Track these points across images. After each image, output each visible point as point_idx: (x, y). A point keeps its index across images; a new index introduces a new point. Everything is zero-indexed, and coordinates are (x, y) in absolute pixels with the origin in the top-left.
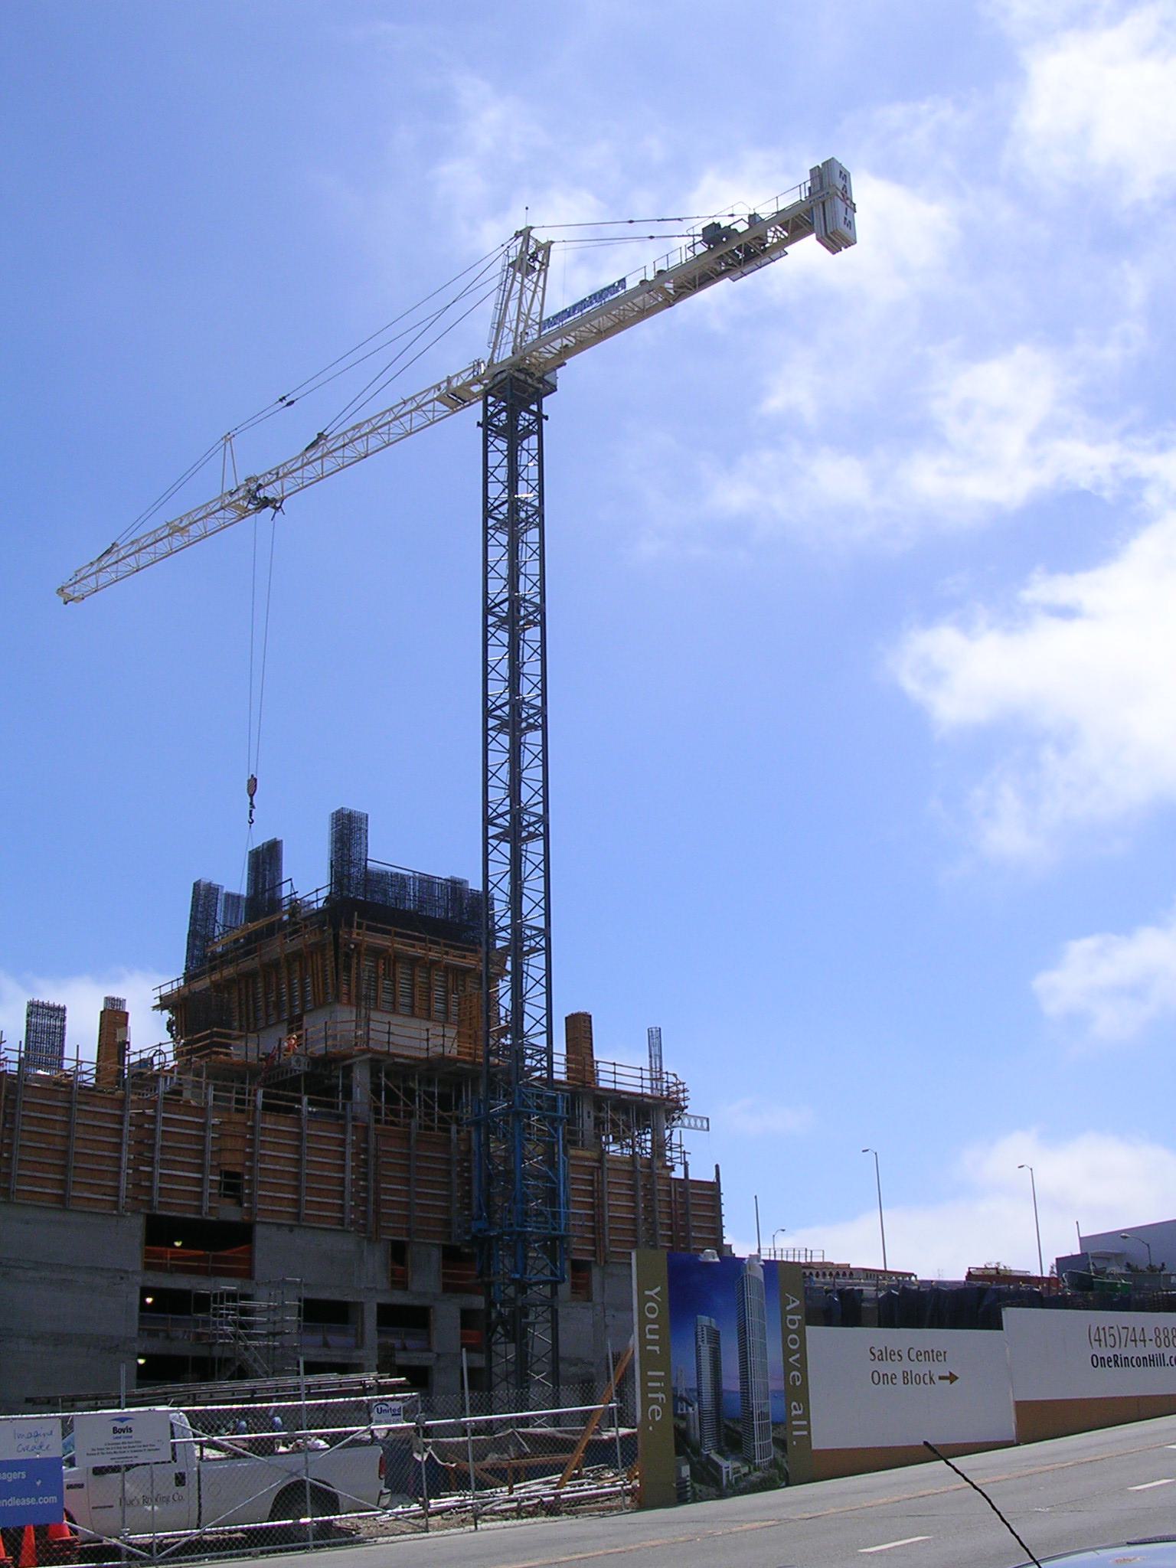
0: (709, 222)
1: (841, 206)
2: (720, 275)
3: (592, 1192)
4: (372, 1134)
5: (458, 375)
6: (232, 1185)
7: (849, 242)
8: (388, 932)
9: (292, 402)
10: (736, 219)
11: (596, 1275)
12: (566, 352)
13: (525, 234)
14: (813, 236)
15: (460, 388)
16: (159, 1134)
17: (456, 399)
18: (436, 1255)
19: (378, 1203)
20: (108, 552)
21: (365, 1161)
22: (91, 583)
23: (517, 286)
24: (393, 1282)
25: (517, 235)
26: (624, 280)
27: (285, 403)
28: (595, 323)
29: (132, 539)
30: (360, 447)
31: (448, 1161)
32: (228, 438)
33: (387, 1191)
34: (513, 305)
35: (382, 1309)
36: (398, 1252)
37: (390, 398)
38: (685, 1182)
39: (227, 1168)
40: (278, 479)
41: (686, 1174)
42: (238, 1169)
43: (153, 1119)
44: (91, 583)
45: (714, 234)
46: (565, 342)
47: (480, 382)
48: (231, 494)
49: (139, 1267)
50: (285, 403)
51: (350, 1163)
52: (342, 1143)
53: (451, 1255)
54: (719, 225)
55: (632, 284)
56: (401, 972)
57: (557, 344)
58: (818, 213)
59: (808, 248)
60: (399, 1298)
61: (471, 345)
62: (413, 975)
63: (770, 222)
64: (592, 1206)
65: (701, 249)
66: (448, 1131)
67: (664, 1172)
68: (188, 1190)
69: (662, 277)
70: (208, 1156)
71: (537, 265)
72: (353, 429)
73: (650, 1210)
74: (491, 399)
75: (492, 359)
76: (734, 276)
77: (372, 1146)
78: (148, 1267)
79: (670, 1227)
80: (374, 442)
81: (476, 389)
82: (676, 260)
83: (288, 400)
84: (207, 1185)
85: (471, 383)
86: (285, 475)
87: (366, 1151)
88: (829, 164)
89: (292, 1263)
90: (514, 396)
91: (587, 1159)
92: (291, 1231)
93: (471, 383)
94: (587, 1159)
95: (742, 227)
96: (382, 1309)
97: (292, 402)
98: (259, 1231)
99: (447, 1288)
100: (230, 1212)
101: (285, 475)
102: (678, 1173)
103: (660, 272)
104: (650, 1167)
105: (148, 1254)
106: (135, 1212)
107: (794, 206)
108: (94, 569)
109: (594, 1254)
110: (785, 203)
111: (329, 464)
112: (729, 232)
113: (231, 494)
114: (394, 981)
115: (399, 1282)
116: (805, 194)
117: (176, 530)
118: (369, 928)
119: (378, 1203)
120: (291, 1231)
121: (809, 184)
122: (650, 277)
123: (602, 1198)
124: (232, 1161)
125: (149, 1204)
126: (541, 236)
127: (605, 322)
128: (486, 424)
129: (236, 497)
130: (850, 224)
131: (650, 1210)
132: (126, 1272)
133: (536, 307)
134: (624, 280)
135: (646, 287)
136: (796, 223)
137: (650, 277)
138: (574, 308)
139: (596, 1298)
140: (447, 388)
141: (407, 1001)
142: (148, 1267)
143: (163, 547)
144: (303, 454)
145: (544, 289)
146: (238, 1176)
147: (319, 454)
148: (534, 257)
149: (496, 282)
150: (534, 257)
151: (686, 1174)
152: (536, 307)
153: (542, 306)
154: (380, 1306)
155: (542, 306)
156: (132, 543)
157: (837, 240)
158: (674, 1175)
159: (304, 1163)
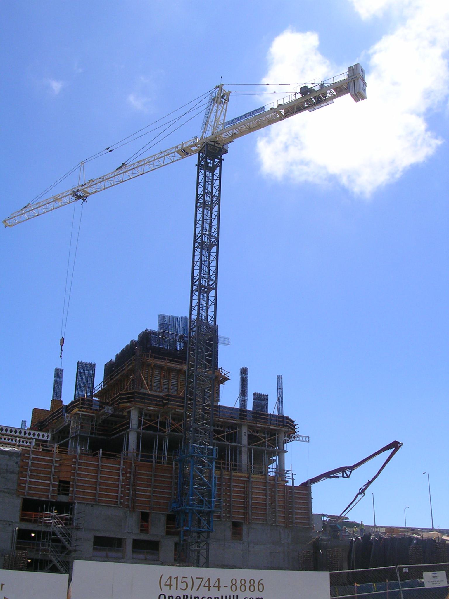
0: (304, 85)
1: (361, 83)
2: (305, 109)
3: (244, 492)
4: (133, 465)
5: (186, 143)
6: (64, 486)
7: (363, 98)
8: (165, 359)
9: (112, 150)
10: (314, 85)
11: (245, 528)
12: (234, 136)
13: (220, 87)
14: (349, 94)
15: (188, 147)
16: (30, 464)
17: (185, 152)
18: (163, 519)
19: (134, 495)
20: (26, 207)
21: (130, 477)
22: (17, 220)
23: (215, 108)
24: (141, 530)
25: (216, 88)
26: (264, 107)
27: (109, 150)
28: (248, 124)
29: (37, 202)
30: (140, 170)
31: (171, 478)
32: (83, 163)
33: (139, 490)
34: (213, 116)
35: (135, 541)
36: (145, 517)
37: (156, 150)
38: (292, 487)
39: (62, 479)
40: (103, 181)
41: (293, 484)
42: (68, 480)
43: (28, 458)
44: (17, 220)
45: (305, 91)
46: (235, 132)
47: (196, 145)
48: (82, 186)
49: (18, 520)
50: (109, 150)
51: (121, 478)
52: (119, 469)
53: (171, 519)
54: (307, 87)
55: (267, 109)
56: (172, 375)
57: (231, 132)
58: (351, 85)
59: (347, 98)
60: (144, 537)
61: (194, 132)
62: (178, 377)
63: (329, 88)
64: (244, 498)
65: (299, 96)
66: (172, 464)
67: (282, 483)
68: (44, 488)
69: (280, 107)
70: (53, 474)
71: (224, 101)
72: (138, 162)
73: (273, 500)
74: (201, 154)
75: (202, 137)
76: (310, 110)
77: (132, 471)
78: (22, 520)
79: (284, 507)
80: (147, 168)
81: (194, 149)
82: (287, 101)
83: (110, 149)
84: (51, 486)
85: (192, 146)
86: (106, 179)
87: (130, 473)
88: (357, 66)
89: (96, 519)
90: (211, 154)
91: (242, 477)
92: (92, 506)
93: (192, 146)
94: (242, 477)
95: (317, 88)
96: (135, 541)
97: (112, 150)
98: (76, 506)
99: (168, 533)
100: (63, 499)
101: (106, 179)
102: (290, 484)
103: (280, 105)
104: (274, 480)
105: (22, 515)
106: (18, 496)
107: (341, 81)
108: (19, 213)
109: (243, 519)
110: (338, 79)
111: (126, 176)
112: (311, 90)
113: (82, 186)
114: (169, 380)
115: (144, 529)
116: (346, 77)
117: (56, 199)
118: (155, 357)
119: (134, 495)
120: (92, 506)
121: (348, 73)
122: (275, 106)
123: (249, 494)
124: (64, 476)
125: (23, 494)
126: (226, 89)
127: (252, 124)
128: (199, 165)
129: (84, 187)
130: (364, 90)
131: (273, 500)
132: (12, 522)
133: (222, 118)
134: (264, 107)
135: (273, 110)
136: (340, 89)
137: (275, 106)
138: (241, 117)
139: (245, 538)
140: (182, 147)
141: (175, 388)
142: (22, 520)
143: (50, 206)
144: (115, 171)
145: (226, 111)
146: (68, 483)
147: (122, 171)
148: (223, 97)
149: (206, 106)
150: (223, 97)
151: (293, 484)
152: (222, 118)
153: (225, 117)
154: (134, 540)
155: (225, 117)
156: (37, 204)
157: (359, 96)
158: (288, 484)
159: (99, 477)
